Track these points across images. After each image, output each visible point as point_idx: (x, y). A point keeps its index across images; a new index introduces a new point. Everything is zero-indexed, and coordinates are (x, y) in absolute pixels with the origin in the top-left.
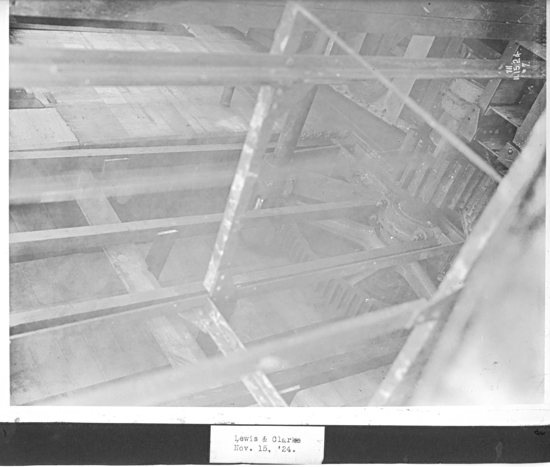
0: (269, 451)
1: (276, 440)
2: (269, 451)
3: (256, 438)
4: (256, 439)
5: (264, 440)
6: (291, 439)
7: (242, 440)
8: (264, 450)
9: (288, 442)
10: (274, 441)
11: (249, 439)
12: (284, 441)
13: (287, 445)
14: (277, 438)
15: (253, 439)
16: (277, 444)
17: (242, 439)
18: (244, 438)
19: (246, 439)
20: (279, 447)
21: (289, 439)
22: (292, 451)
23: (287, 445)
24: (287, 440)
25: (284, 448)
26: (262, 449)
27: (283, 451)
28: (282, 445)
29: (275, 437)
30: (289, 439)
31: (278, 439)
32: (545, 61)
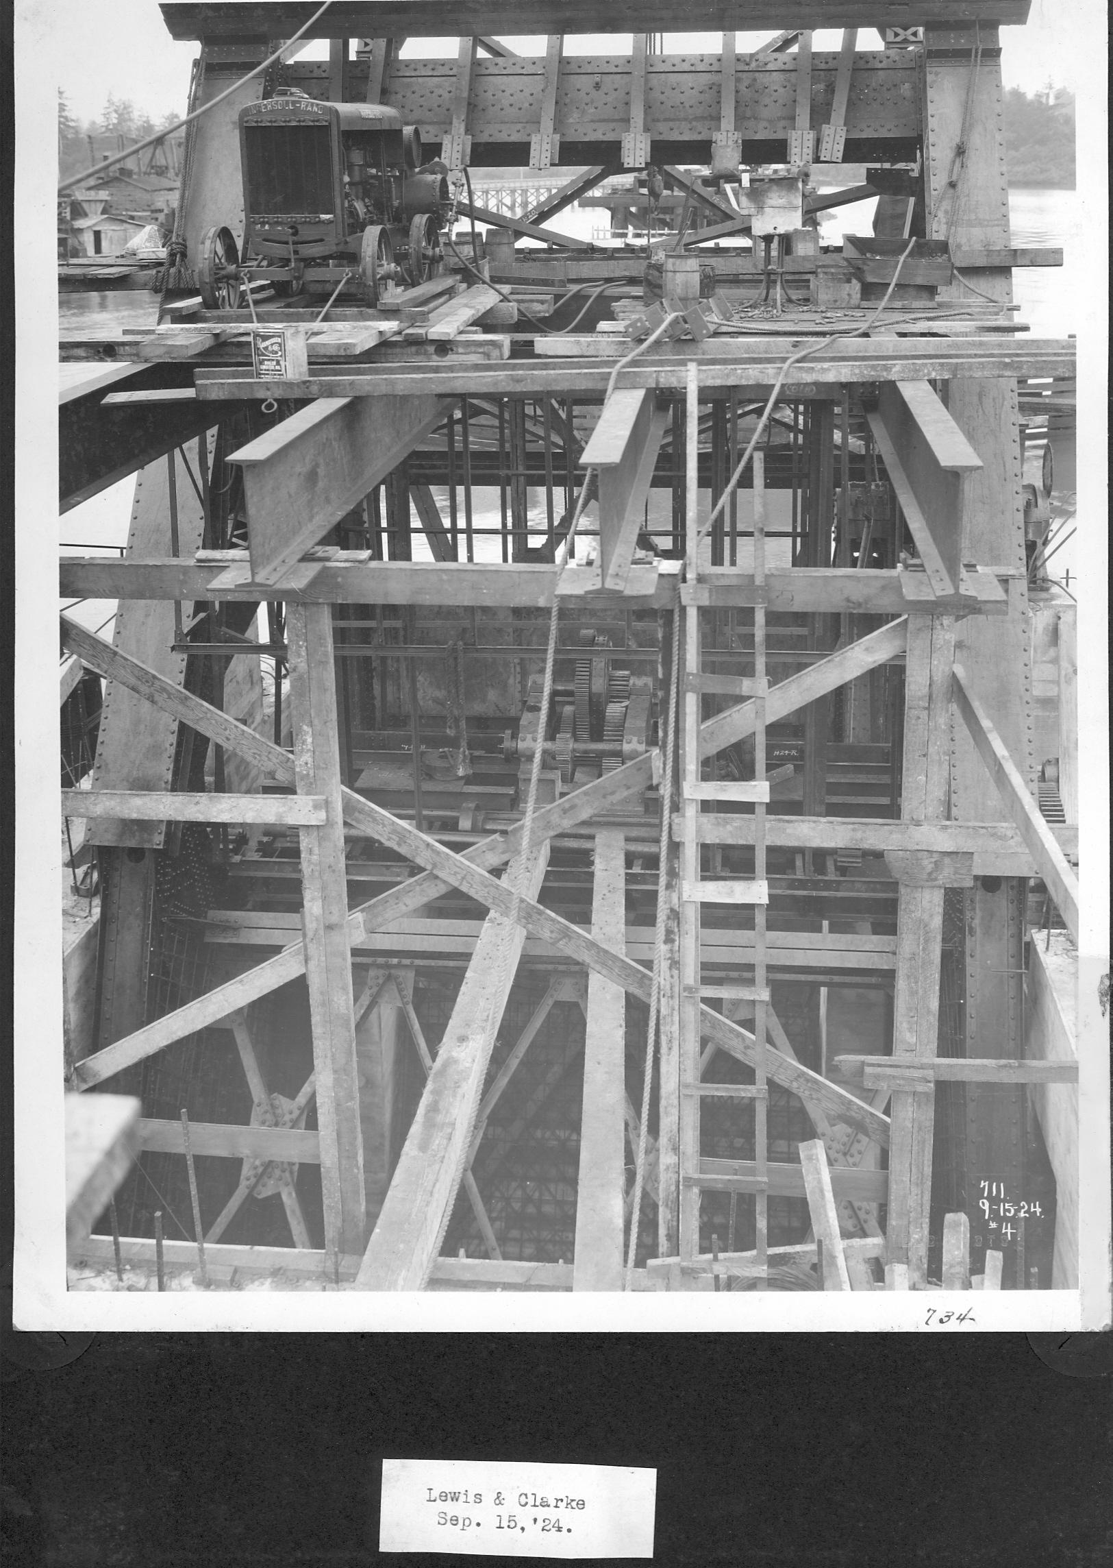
0: (523, 1529)
1: (527, 1503)
2: (523, 1529)
3: (443, 1515)
4: (478, 1498)
5: (497, 1502)
6: (562, 1500)
7: (443, 1498)
8: (509, 1527)
9: (556, 1507)
10: (523, 1503)
11: (462, 1498)
12: (545, 1504)
13: (551, 1513)
14: (529, 1495)
15: (471, 1498)
16: (531, 1512)
17: (444, 1497)
18: (449, 1496)
19: (455, 1497)
20: (535, 1520)
21: (557, 1500)
22: (564, 1530)
23: (551, 1513)
24: (553, 1503)
25: (547, 1522)
26: (505, 1524)
27: (543, 1530)
28: (541, 1513)
29: (526, 1495)
30: (557, 1500)
31: (531, 1500)
32: (271, 1162)
